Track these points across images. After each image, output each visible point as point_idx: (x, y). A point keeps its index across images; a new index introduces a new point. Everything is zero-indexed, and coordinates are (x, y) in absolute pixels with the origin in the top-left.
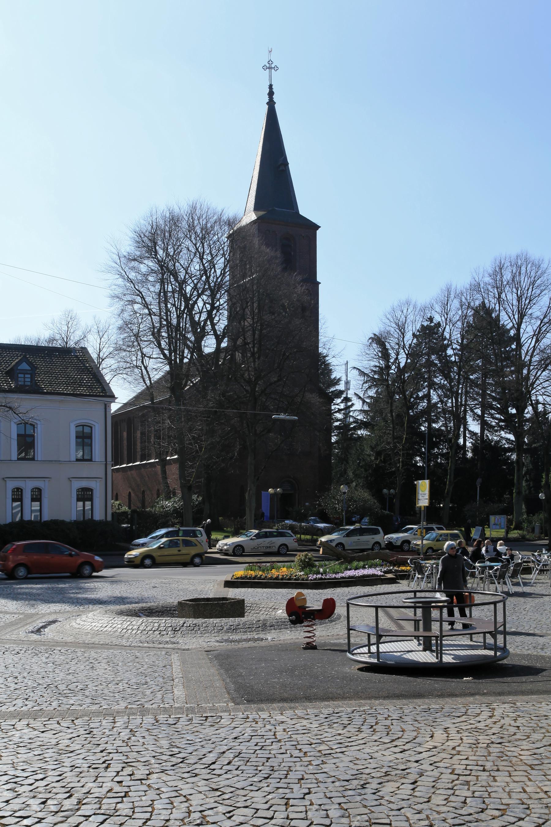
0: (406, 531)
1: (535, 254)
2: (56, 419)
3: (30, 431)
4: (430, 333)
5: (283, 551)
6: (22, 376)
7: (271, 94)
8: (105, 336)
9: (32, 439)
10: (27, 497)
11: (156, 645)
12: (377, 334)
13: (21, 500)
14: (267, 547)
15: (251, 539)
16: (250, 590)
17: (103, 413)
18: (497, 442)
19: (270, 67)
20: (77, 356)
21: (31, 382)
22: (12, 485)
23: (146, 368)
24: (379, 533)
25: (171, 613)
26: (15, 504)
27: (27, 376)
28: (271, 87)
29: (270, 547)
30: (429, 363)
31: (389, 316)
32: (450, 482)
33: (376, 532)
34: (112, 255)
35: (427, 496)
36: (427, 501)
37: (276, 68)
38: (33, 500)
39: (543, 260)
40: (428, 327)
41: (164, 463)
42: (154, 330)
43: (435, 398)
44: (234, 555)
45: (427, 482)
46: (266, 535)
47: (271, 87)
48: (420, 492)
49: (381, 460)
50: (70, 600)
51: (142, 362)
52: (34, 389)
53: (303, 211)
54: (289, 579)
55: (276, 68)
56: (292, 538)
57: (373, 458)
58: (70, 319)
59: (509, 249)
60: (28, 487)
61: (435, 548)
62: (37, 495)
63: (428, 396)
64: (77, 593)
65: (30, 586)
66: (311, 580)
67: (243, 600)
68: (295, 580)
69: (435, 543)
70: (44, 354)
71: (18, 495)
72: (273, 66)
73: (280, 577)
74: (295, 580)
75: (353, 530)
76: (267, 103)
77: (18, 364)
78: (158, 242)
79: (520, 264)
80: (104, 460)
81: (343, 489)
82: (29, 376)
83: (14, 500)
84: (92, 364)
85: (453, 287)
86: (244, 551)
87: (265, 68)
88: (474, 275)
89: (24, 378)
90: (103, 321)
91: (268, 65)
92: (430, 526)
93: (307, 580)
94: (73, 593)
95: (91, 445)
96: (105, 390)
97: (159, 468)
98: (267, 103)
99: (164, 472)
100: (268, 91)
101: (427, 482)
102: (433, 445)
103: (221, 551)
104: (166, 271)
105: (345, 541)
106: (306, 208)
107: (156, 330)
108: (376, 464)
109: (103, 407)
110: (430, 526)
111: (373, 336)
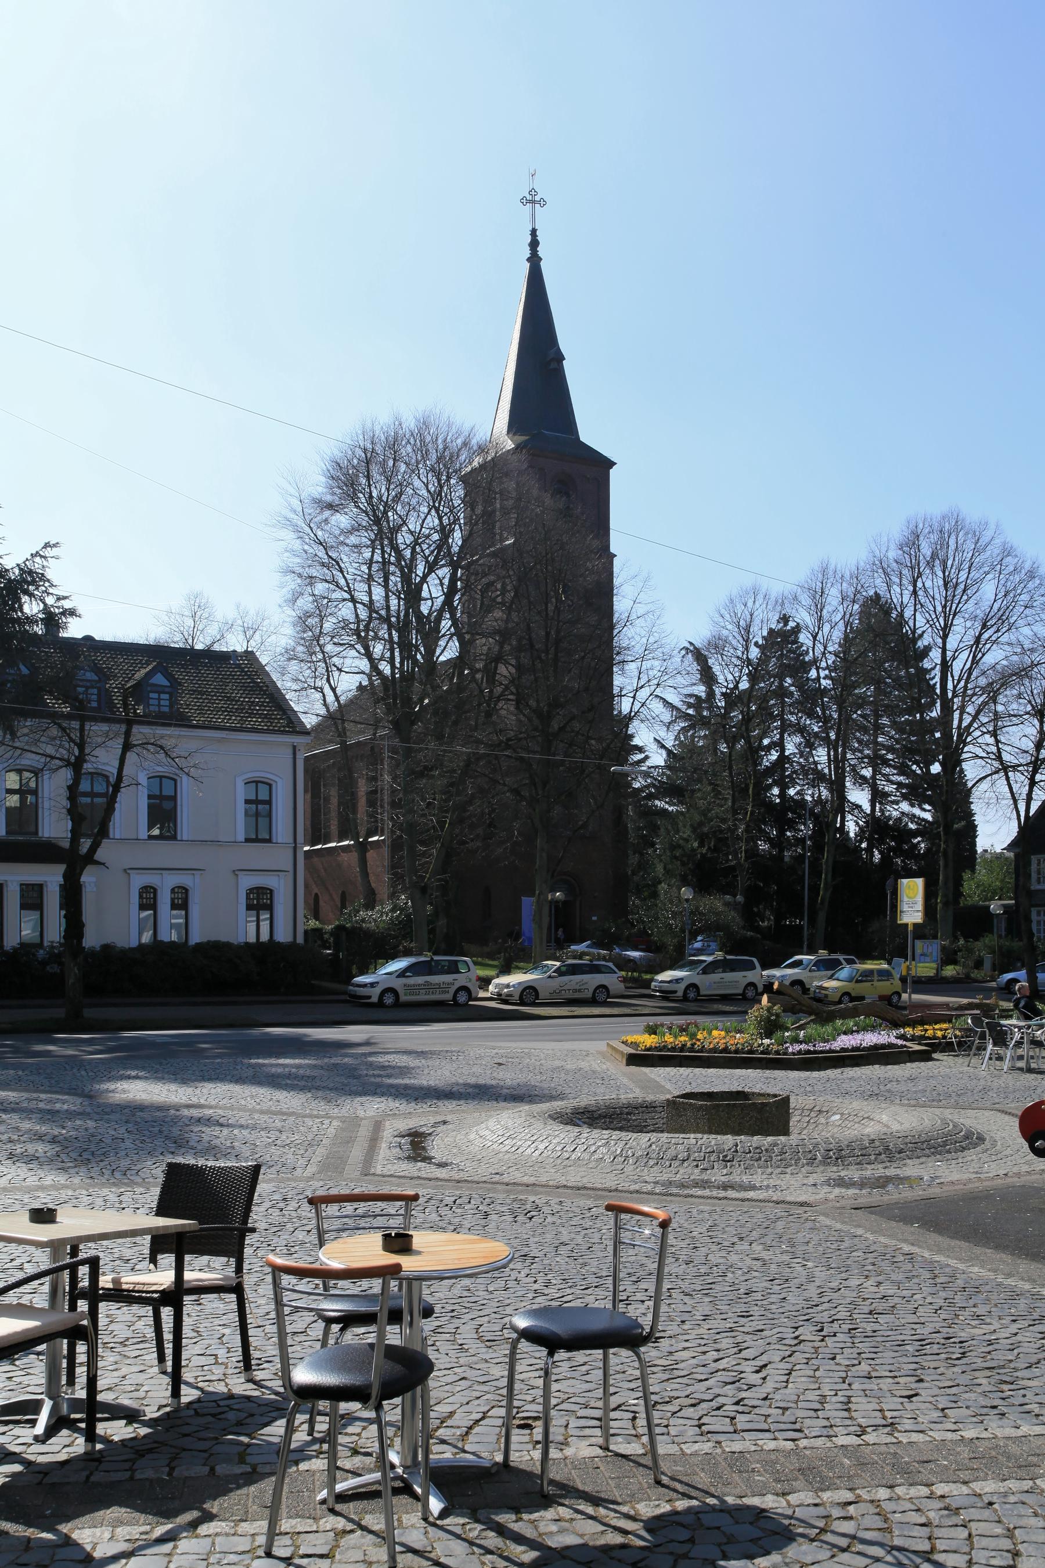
0: (798, 964)
1: (972, 513)
2: (219, 772)
3: (168, 791)
4: (782, 640)
5: (601, 997)
6: (156, 696)
7: (534, 244)
8: (257, 636)
9: (172, 804)
10: (164, 900)
11: (675, 1190)
12: (698, 645)
13: (153, 907)
14: (575, 991)
15: (550, 977)
16: (697, 1070)
17: (290, 761)
18: (899, 820)
19: (532, 200)
20: (239, 666)
21: (171, 706)
22: (139, 881)
23: (334, 690)
24: (754, 968)
25: (625, 1119)
26: (145, 914)
27: (163, 696)
28: (534, 232)
29: (580, 991)
30: (782, 693)
31: (723, 611)
32: (826, 884)
33: (751, 967)
34: (290, 499)
35: (920, 906)
36: (920, 914)
37: (542, 203)
38: (174, 906)
39: (987, 523)
40: (781, 633)
41: (363, 848)
42: (358, 626)
43: (790, 748)
44: (522, 1003)
45: (920, 882)
46: (573, 970)
47: (534, 232)
48: (906, 899)
49: (709, 848)
50: (393, 1090)
51: (328, 680)
52: (177, 719)
53: (586, 436)
54: (751, 1052)
55: (542, 203)
56: (616, 975)
57: (696, 844)
58: (198, 610)
59: (932, 506)
60: (166, 884)
61: (853, 995)
62: (181, 900)
63: (780, 745)
64: (380, 1076)
65: (281, 1061)
66: (794, 1054)
67: (786, 1100)
68: (762, 1053)
69: (852, 985)
70: (186, 661)
71: (148, 899)
72: (537, 198)
73: (733, 1048)
74: (762, 1053)
75: (712, 963)
76: (528, 260)
77: (149, 675)
78: (364, 479)
79: (950, 529)
80: (291, 840)
81: (685, 894)
82: (167, 696)
83: (142, 907)
84: (266, 679)
85: (832, 567)
86: (537, 997)
87: (524, 201)
88: (873, 545)
89: (159, 699)
90: (252, 612)
91: (529, 197)
92: (834, 956)
93: (785, 1054)
94: (374, 1076)
95: (270, 815)
96: (292, 723)
97: (354, 856)
98: (528, 260)
99: (363, 862)
100: (529, 239)
101: (920, 882)
102: (784, 823)
103: (500, 998)
104: (382, 528)
105: (398, 984)
106: (592, 431)
107: (362, 627)
108: (702, 854)
109: (290, 751)
110: (834, 956)
111: (688, 645)
